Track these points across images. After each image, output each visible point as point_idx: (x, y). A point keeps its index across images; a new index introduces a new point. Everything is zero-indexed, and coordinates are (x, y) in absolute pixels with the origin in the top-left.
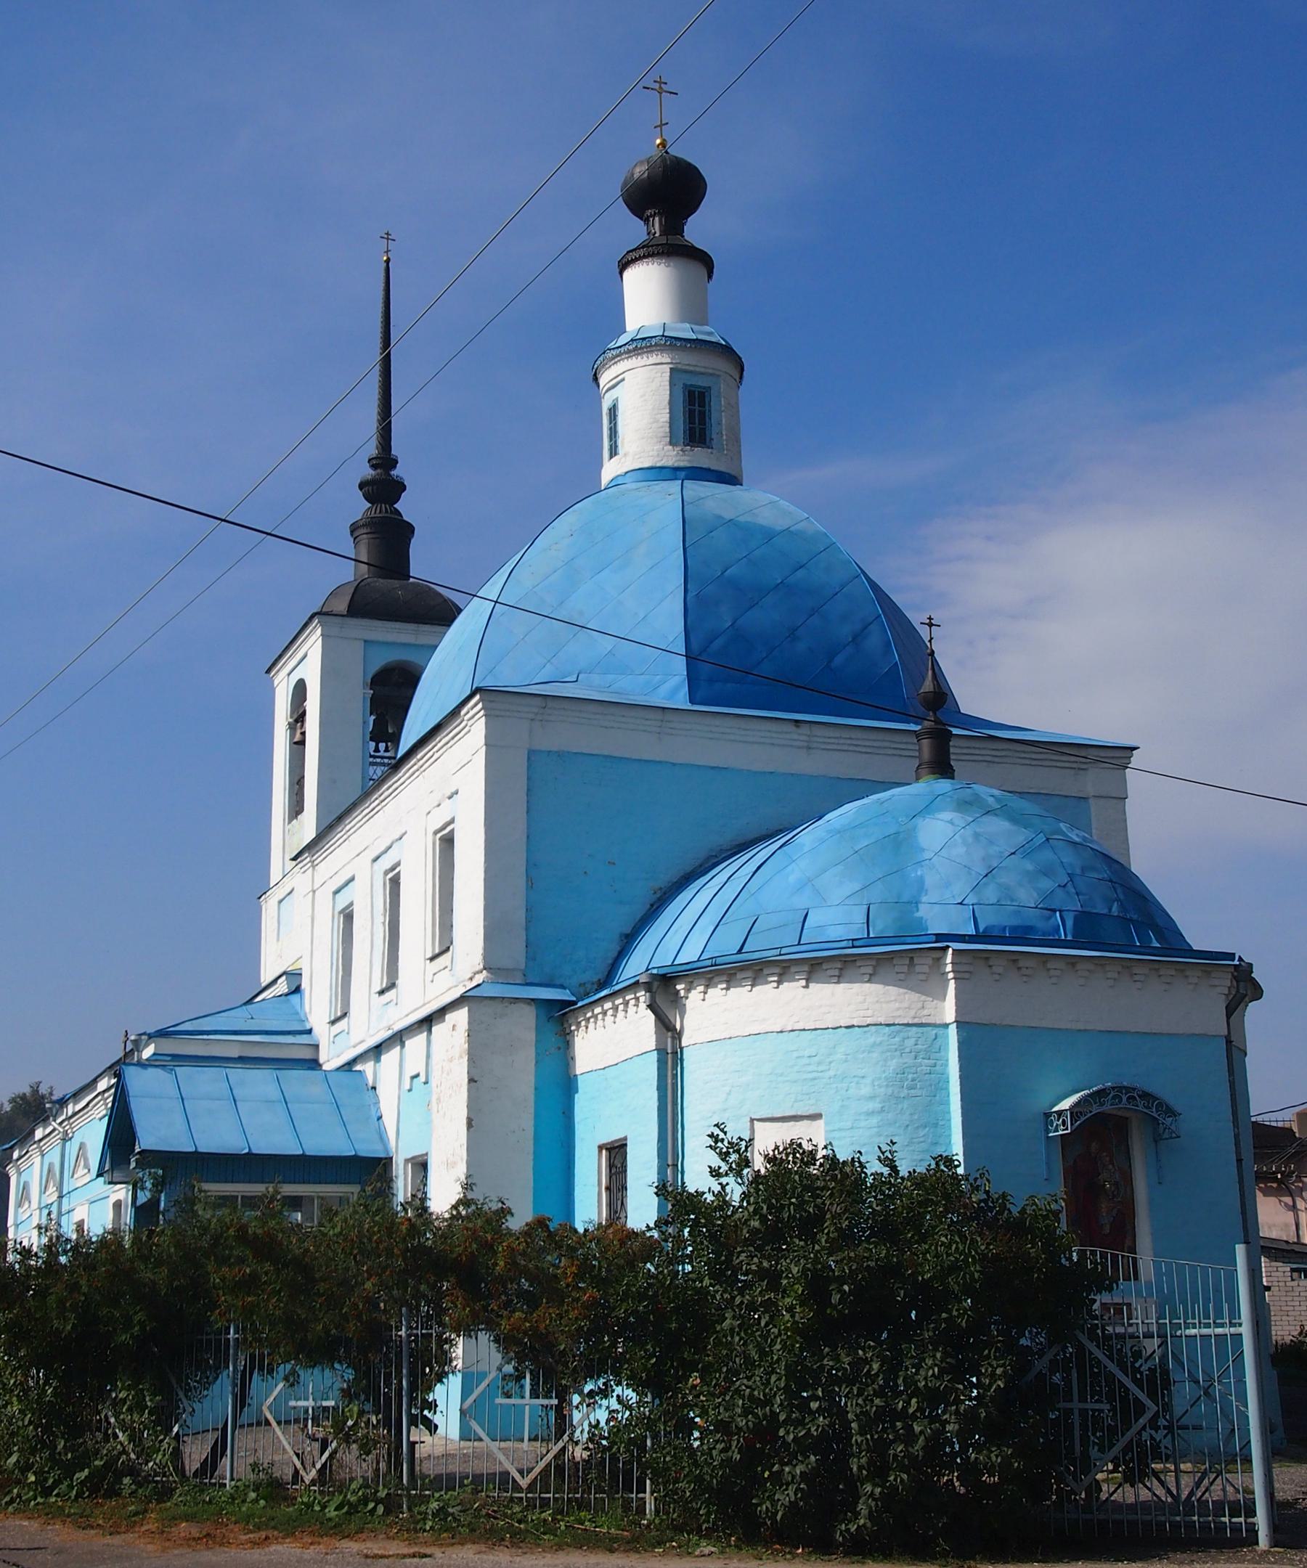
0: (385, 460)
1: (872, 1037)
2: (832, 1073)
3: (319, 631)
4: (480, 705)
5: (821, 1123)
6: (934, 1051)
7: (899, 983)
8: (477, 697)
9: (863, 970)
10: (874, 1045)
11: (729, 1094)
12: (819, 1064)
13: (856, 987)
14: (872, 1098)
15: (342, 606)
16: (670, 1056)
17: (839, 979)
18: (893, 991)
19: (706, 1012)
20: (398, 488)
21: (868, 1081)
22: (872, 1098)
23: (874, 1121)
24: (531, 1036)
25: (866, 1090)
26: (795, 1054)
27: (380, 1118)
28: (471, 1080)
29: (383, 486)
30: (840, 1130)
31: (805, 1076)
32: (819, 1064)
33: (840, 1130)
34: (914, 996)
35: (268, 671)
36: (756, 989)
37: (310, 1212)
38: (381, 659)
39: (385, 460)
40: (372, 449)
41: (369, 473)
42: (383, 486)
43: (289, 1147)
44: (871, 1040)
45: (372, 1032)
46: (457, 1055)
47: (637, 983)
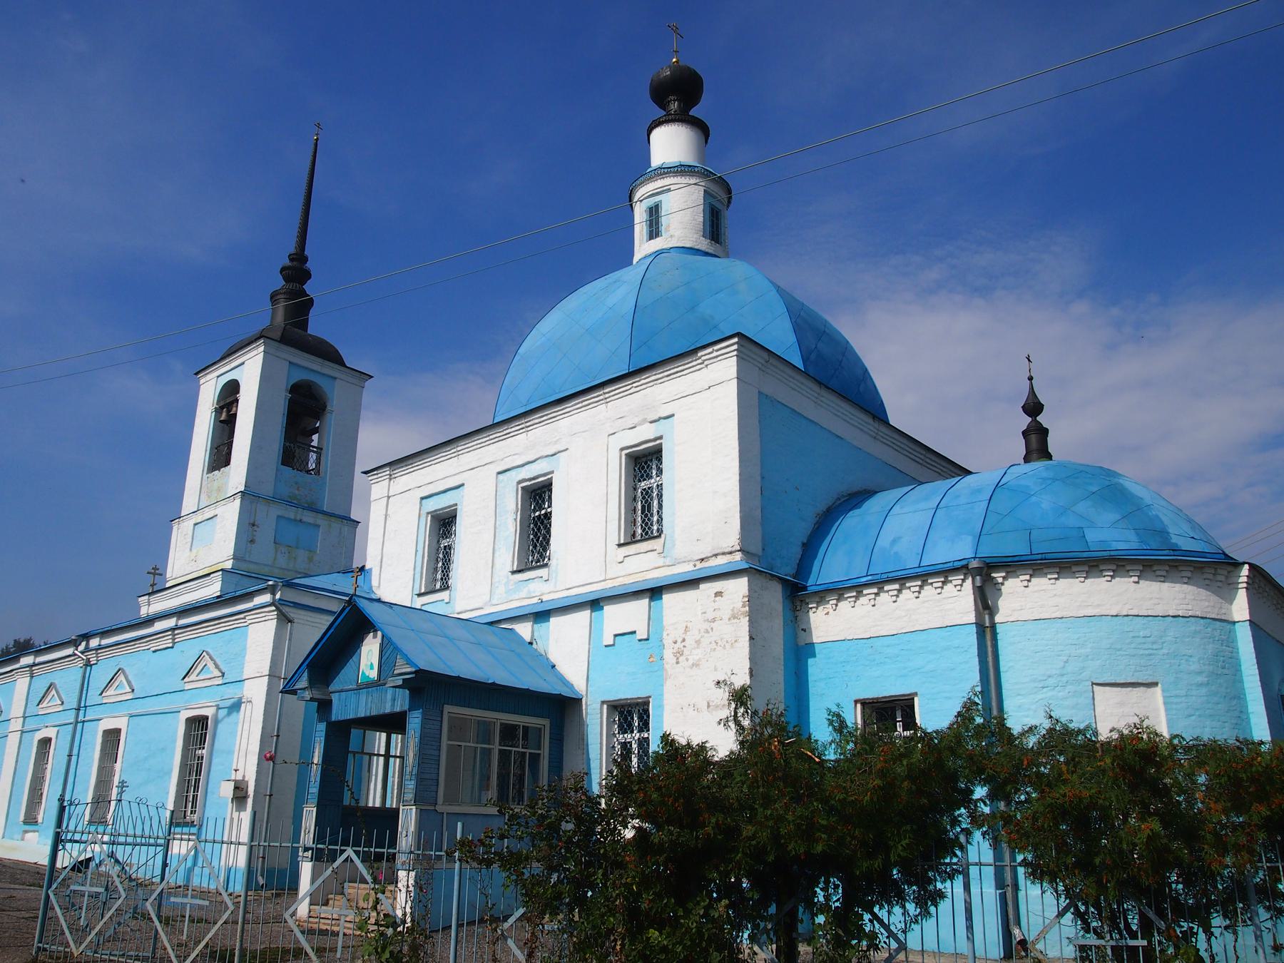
0: (299, 257)
1: (1193, 626)
2: (1165, 651)
3: (262, 348)
4: (735, 347)
5: (1158, 690)
6: (1230, 641)
7: (1207, 587)
8: (736, 340)
9: (1184, 574)
10: (1195, 632)
11: (1066, 662)
12: (1153, 643)
13: (1178, 587)
14: (1200, 673)
15: (278, 335)
16: (986, 631)
17: (1164, 579)
18: (1203, 593)
19: (1021, 598)
20: (307, 275)
21: (1195, 659)
22: (1200, 673)
23: (1204, 690)
24: (780, 607)
25: (1194, 667)
26: (1131, 634)
27: (554, 666)
28: (751, 638)
29: (297, 272)
30: (1177, 696)
31: (1142, 652)
32: (1153, 643)
33: (1177, 696)
34: (1214, 598)
35: (197, 374)
36: (1089, 581)
37: (1136, 738)
38: (299, 376)
39: (299, 257)
40: (291, 247)
41: (287, 262)
42: (297, 272)
43: (1002, 669)
44: (1193, 628)
45: (494, 602)
46: (726, 614)
47: (966, 567)
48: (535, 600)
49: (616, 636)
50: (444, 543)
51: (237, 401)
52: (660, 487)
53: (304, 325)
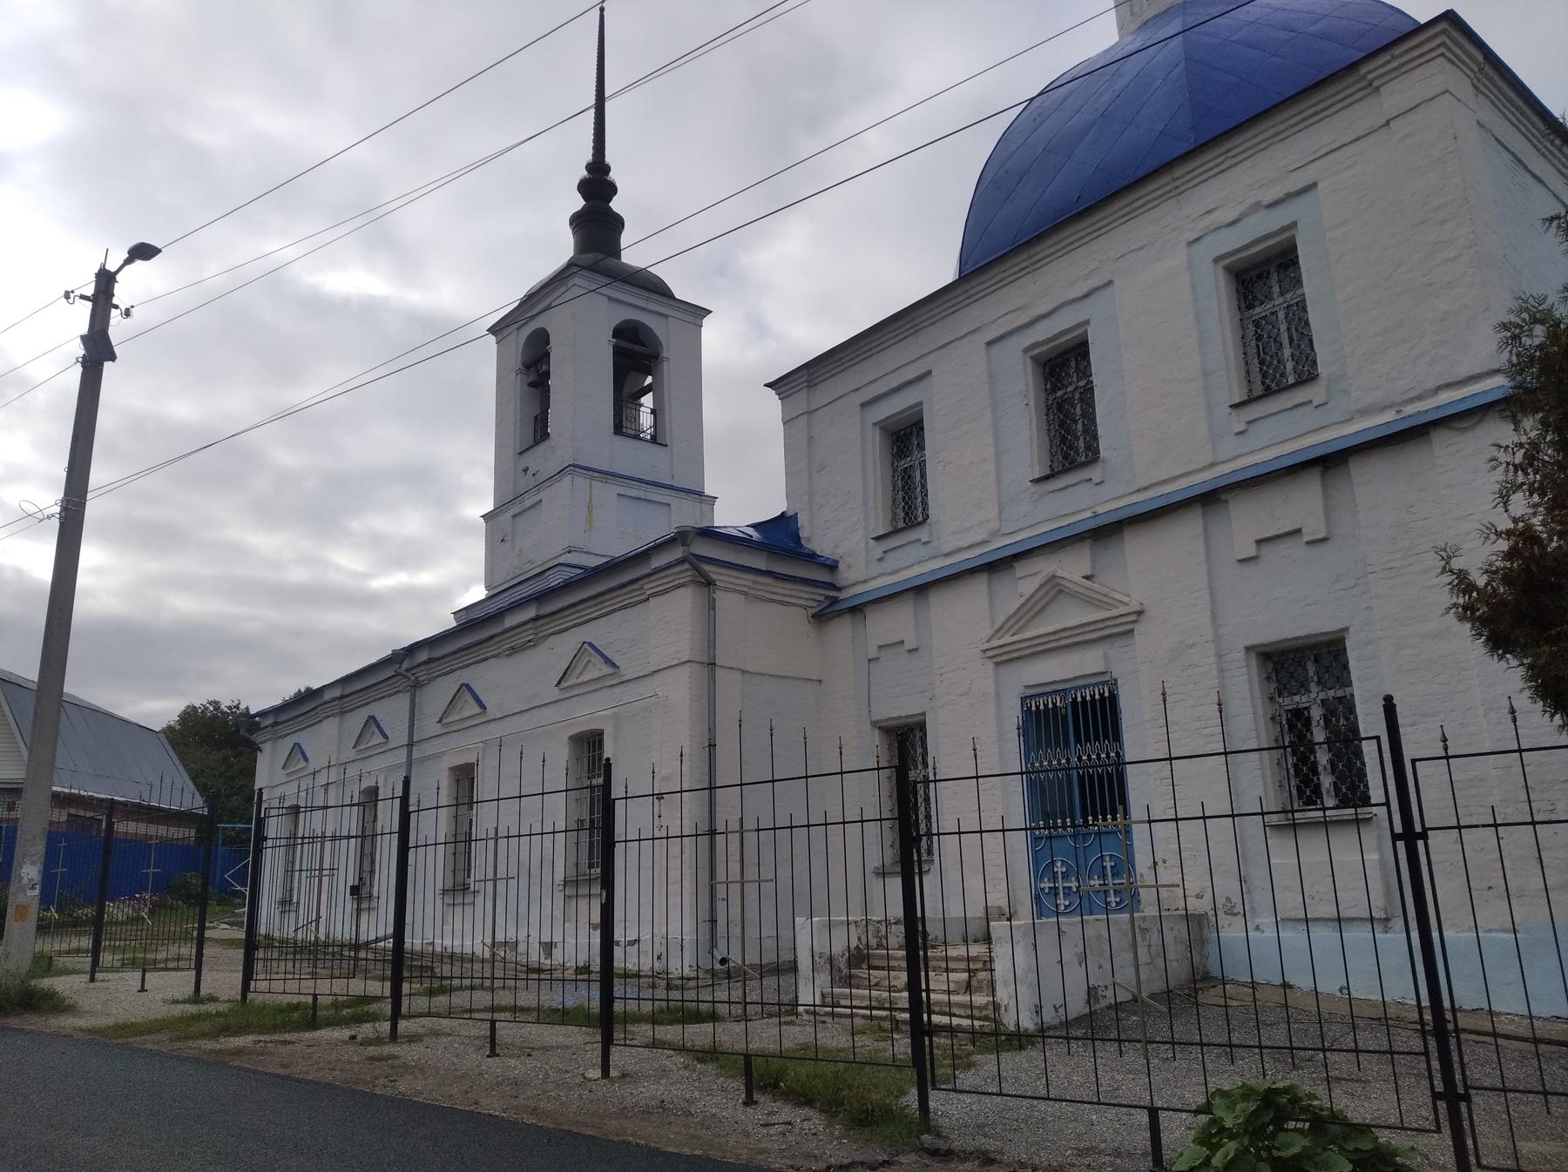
29: (597, 182)
40: (588, 155)
48: (1088, 514)
49: (1259, 542)
50: (904, 464)
51: (548, 355)
52: (923, 464)
53: (617, 253)
